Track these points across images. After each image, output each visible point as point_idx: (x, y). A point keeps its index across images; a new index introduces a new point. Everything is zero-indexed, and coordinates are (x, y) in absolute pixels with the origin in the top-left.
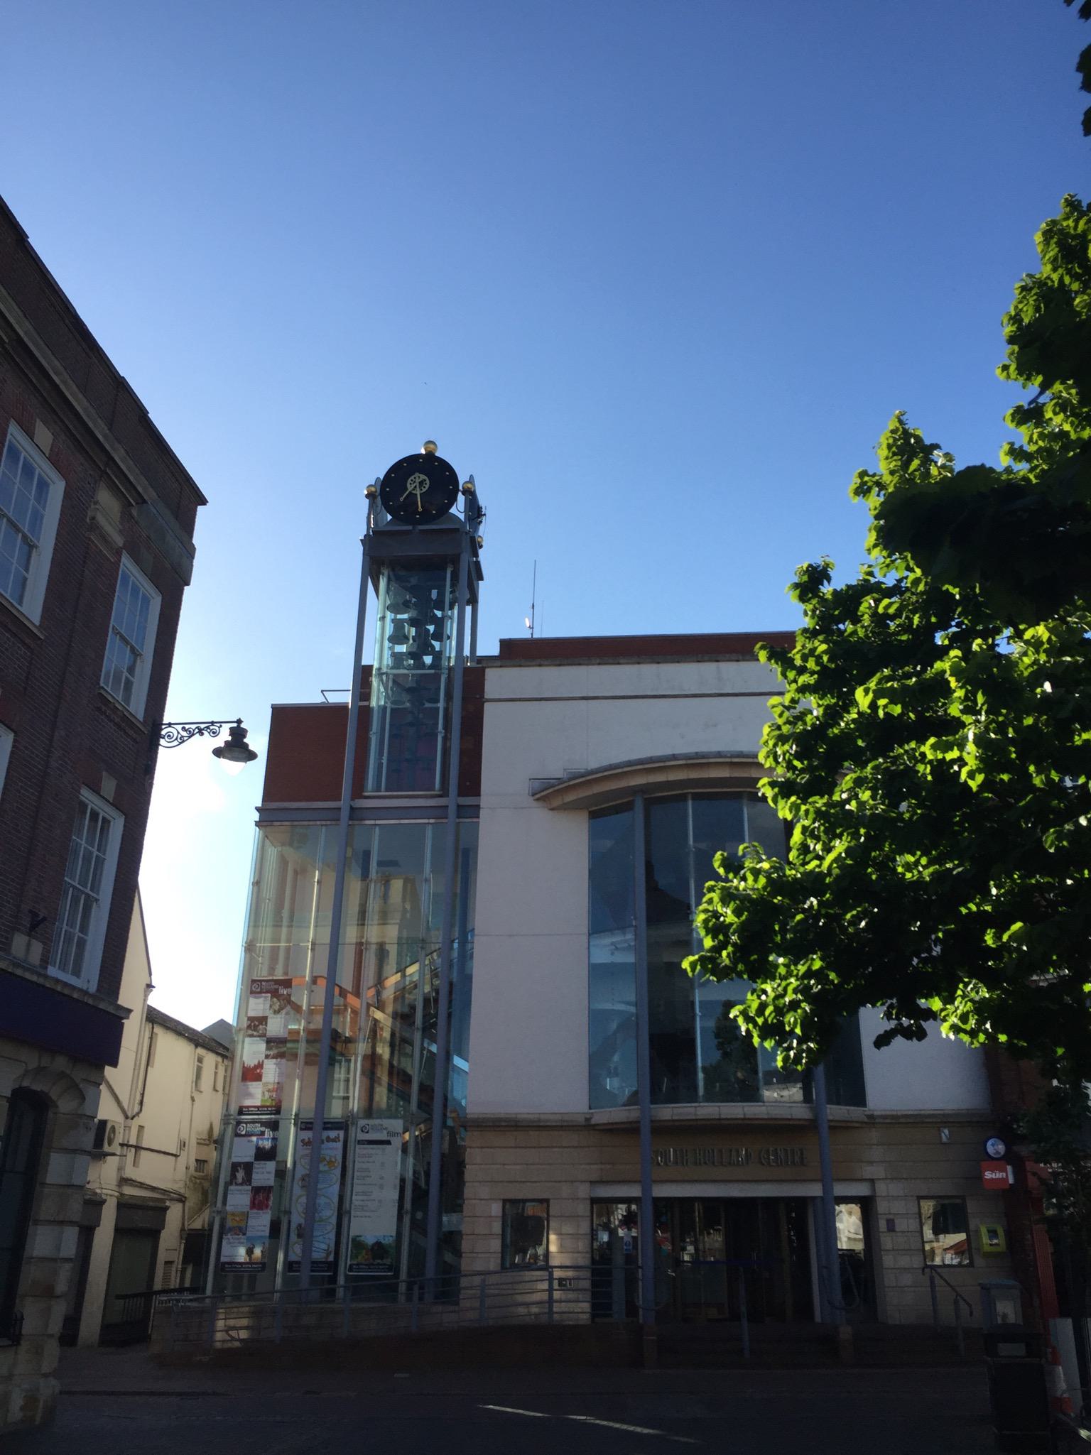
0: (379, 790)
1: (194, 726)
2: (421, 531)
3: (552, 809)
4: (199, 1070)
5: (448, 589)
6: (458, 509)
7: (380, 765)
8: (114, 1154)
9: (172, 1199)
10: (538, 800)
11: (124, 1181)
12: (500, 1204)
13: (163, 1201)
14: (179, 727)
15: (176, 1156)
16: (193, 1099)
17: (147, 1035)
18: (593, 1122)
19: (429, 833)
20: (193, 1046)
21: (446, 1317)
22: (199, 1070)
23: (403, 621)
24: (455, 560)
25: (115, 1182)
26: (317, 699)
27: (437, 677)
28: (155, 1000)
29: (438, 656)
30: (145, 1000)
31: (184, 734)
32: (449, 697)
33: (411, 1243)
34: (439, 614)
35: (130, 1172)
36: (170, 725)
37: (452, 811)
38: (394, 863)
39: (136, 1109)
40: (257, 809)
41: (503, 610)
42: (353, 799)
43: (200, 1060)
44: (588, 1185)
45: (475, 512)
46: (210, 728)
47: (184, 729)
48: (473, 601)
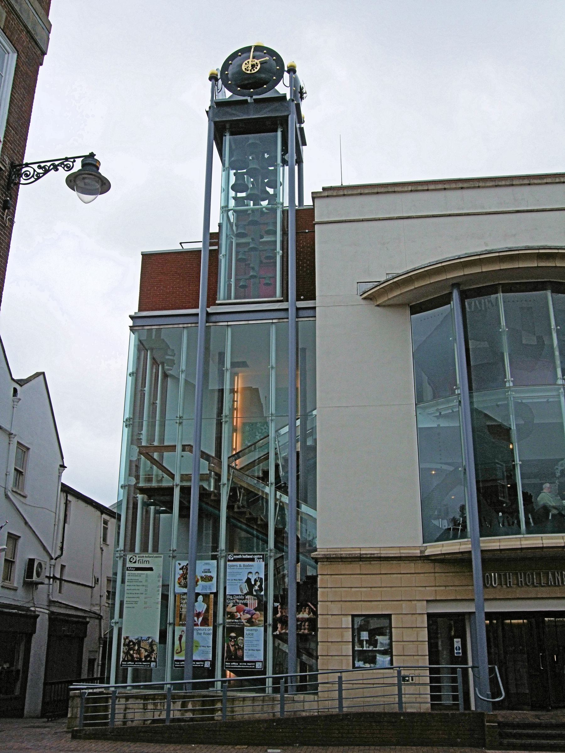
0: (229, 298)
1: (49, 164)
2: (254, 109)
3: (378, 306)
4: (105, 529)
5: (239, 524)
6: (283, 88)
7: (229, 286)
8: (42, 583)
9: (90, 617)
10: (365, 299)
11: (51, 603)
12: (350, 618)
13: (85, 618)
14: (35, 166)
15: (91, 587)
16: (102, 550)
17: (63, 501)
18: (427, 553)
19: (273, 329)
20: (99, 513)
21: (307, 705)
22: (105, 529)
23: (243, 174)
24: (284, 121)
25: (46, 603)
26: (178, 248)
27: (274, 211)
28: (66, 479)
29: (273, 198)
30: (60, 477)
31: (41, 171)
32: (285, 233)
33: (274, 648)
34: (271, 191)
35: (56, 598)
36: (27, 165)
37: (292, 313)
38: (244, 364)
39: (59, 553)
40: (132, 317)
41: (325, 163)
42: (208, 306)
43: (106, 522)
44: (425, 602)
45: (299, 93)
46: (65, 163)
47: (40, 167)
48: (299, 161)
